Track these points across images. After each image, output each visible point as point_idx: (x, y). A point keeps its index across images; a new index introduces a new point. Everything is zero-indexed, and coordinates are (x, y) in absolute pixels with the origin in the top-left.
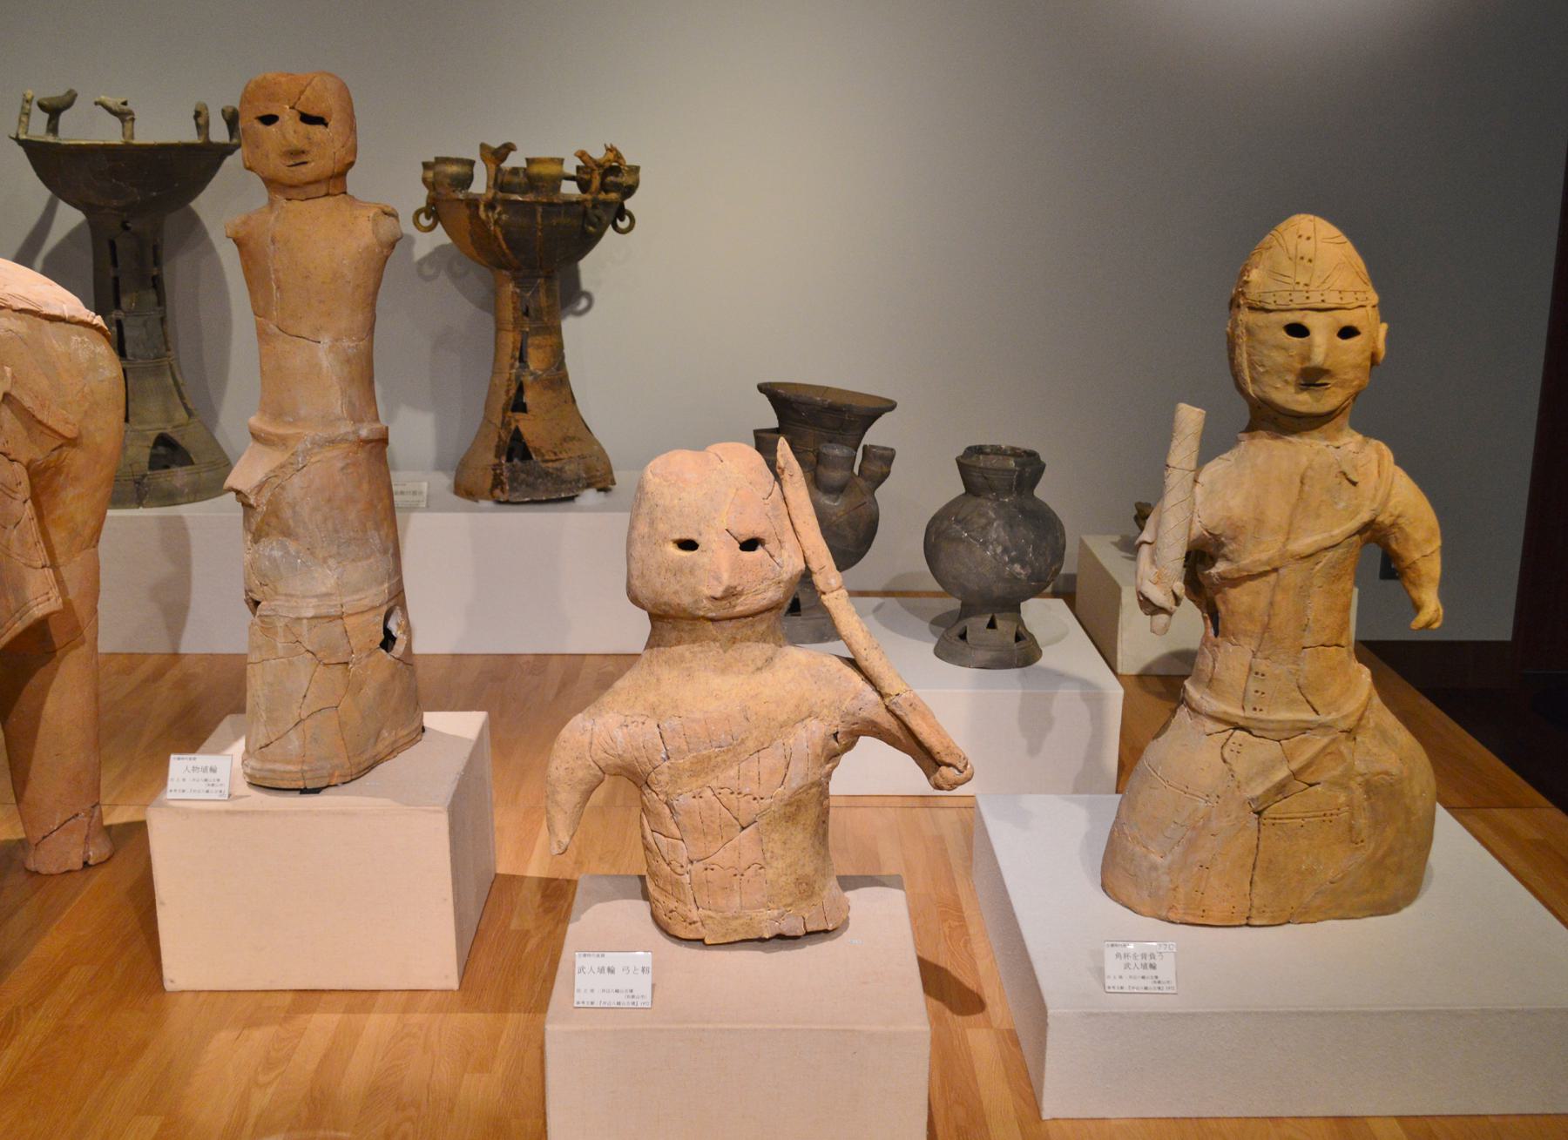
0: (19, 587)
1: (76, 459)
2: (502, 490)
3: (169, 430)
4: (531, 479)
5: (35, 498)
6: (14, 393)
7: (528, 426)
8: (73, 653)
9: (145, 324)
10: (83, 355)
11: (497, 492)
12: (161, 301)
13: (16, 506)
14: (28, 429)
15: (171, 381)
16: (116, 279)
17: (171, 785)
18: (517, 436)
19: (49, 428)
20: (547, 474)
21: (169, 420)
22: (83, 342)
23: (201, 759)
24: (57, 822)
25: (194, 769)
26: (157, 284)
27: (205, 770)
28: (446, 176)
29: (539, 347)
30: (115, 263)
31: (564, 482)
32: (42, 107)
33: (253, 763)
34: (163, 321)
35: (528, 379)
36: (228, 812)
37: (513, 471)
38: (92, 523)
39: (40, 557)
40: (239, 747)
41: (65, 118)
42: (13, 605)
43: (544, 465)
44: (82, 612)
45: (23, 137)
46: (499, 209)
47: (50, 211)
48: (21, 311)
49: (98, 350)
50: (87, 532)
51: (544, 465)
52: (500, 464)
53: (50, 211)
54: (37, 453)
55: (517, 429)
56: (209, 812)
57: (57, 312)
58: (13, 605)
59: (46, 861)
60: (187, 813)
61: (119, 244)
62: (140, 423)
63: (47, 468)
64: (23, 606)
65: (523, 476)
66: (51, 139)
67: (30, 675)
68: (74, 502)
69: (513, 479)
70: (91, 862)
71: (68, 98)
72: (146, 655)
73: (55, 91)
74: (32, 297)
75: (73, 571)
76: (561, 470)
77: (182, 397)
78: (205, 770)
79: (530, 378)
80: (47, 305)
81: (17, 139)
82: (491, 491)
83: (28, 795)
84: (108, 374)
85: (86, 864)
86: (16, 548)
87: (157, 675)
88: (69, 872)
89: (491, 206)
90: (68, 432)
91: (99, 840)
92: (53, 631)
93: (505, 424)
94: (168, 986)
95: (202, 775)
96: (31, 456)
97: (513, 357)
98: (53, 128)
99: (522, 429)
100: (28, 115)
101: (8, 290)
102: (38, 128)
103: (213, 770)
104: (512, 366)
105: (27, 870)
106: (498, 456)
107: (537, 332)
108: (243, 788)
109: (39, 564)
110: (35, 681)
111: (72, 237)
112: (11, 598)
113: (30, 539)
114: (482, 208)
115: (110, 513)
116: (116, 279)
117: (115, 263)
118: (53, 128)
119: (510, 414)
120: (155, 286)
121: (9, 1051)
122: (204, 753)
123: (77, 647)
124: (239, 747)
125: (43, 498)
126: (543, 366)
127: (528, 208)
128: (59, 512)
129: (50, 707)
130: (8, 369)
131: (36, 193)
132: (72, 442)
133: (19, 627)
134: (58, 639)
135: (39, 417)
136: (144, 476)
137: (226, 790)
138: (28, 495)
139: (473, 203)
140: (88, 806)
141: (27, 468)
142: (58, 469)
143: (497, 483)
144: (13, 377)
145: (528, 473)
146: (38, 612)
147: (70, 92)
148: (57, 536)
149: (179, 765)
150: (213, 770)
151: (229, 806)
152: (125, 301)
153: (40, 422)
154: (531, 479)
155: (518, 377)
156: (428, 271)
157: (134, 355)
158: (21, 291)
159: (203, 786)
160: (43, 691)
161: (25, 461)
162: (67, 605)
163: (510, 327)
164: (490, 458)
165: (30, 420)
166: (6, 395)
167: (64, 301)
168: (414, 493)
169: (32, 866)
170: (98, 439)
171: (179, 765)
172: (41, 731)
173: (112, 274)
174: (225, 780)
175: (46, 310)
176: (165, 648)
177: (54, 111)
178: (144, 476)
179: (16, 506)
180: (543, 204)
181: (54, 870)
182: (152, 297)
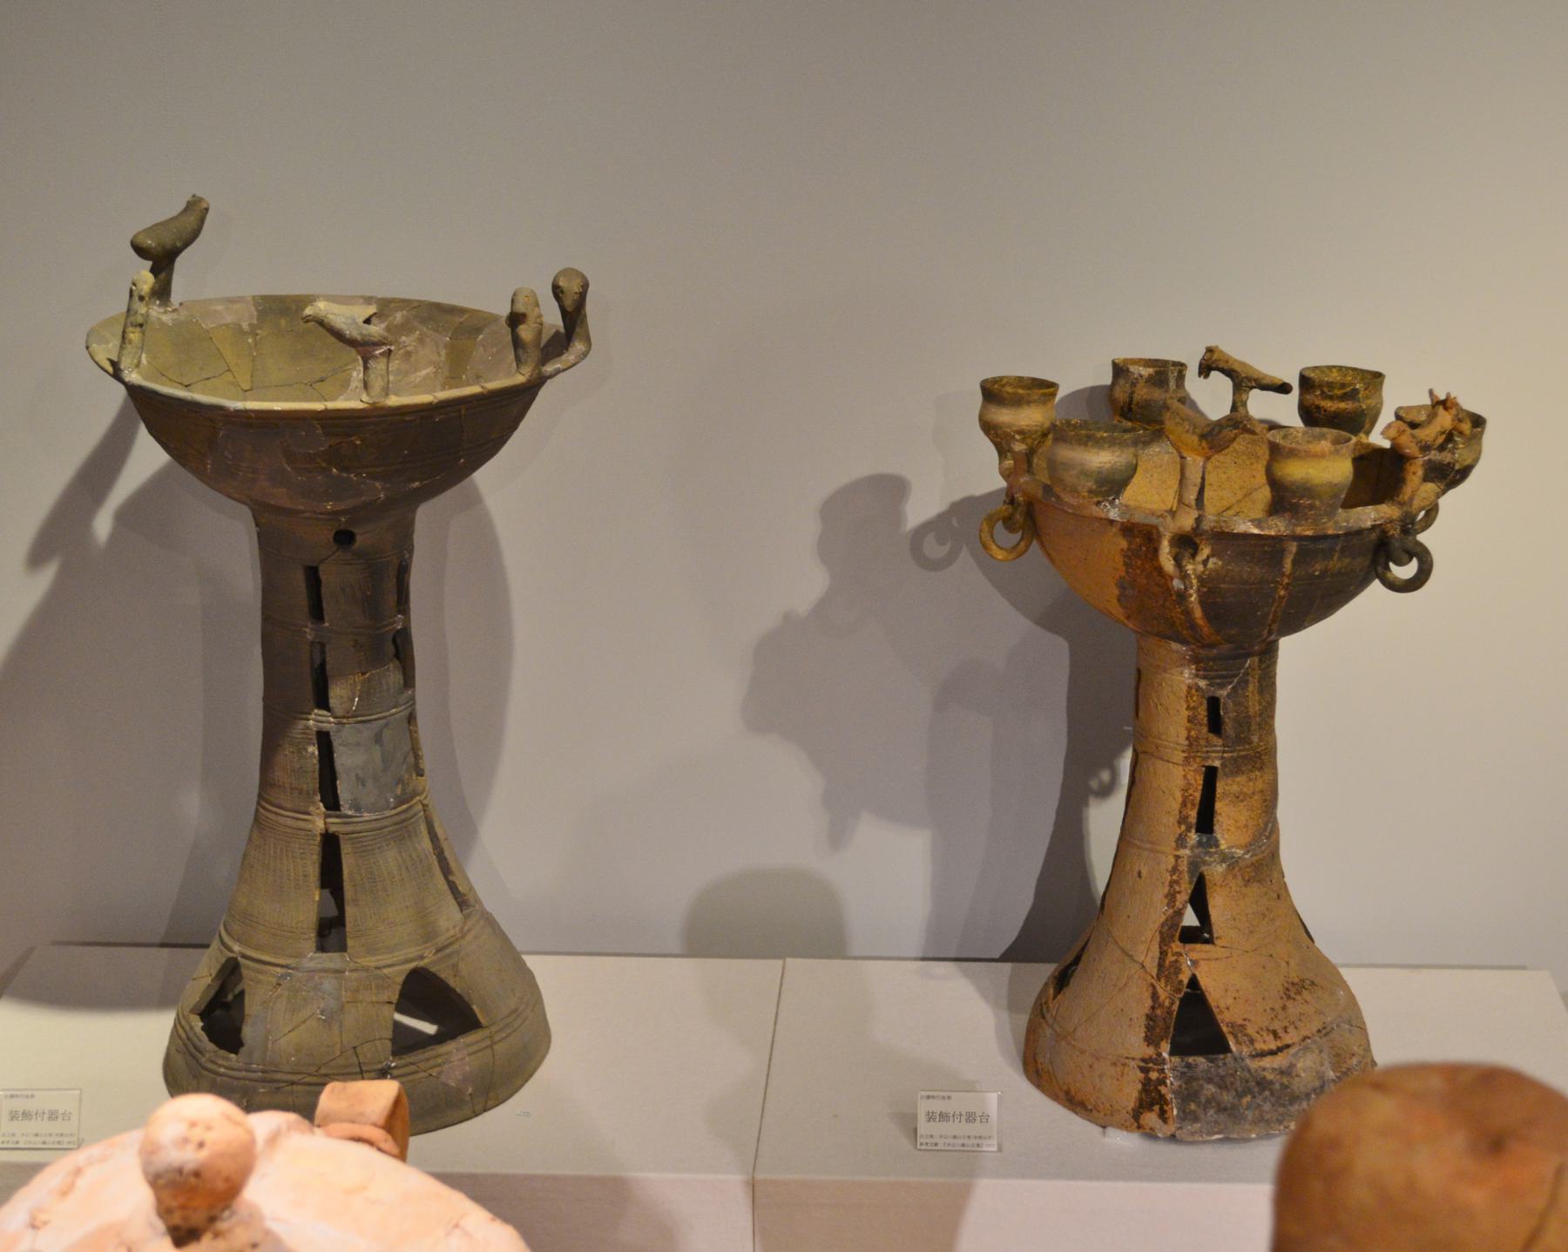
2: (1163, 1115)
3: (428, 960)
4: (1227, 1098)
7: (1222, 976)
9: (378, 739)
11: (1151, 1118)
12: (409, 681)
15: (426, 844)
18: (1194, 997)
20: (1263, 1084)
21: (429, 934)
26: (401, 650)
28: (1085, 473)
29: (1238, 798)
30: (317, 613)
31: (1294, 1099)
34: (411, 718)
35: (1215, 871)
37: (1188, 1076)
43: (1254, 1064)
46: (1205, 551)
51: (1254, 1064)
52: (1159, 1061)
55: (1194, 982)
61: (328, 576)
62: (372, 950)
65: (1210, 1089)
69: (1188, 1095)
71: (192, 219)
73: (159, 208)
76: (1286, 1072)
77: (446, 871)
79: (1221, 869)
82: (1137, 1114)
89: (1186, 543)
93: (1166, 969)
97: (1182, 820)
99: (1204, 982)
104: (1181, 841)
106: (1151, 1040)
107: (1236, 767)
114: (1165, 547)
119: (1177, 946)
120: (397, 656)
126: (1244, 838)
127: (1269, 549)
139: (1142, 536)
143: (1151, 1098)
145: (1223, 1086)
152: (338, 693)
154: (1227, 1098)
155: (1194, 865)
156: (933, 549)
157: (357, 808)
163: (1179, 756)
164: (1136, 1045)
168: (971, 1118)
180: (1300, 538)
182: (394, 677)
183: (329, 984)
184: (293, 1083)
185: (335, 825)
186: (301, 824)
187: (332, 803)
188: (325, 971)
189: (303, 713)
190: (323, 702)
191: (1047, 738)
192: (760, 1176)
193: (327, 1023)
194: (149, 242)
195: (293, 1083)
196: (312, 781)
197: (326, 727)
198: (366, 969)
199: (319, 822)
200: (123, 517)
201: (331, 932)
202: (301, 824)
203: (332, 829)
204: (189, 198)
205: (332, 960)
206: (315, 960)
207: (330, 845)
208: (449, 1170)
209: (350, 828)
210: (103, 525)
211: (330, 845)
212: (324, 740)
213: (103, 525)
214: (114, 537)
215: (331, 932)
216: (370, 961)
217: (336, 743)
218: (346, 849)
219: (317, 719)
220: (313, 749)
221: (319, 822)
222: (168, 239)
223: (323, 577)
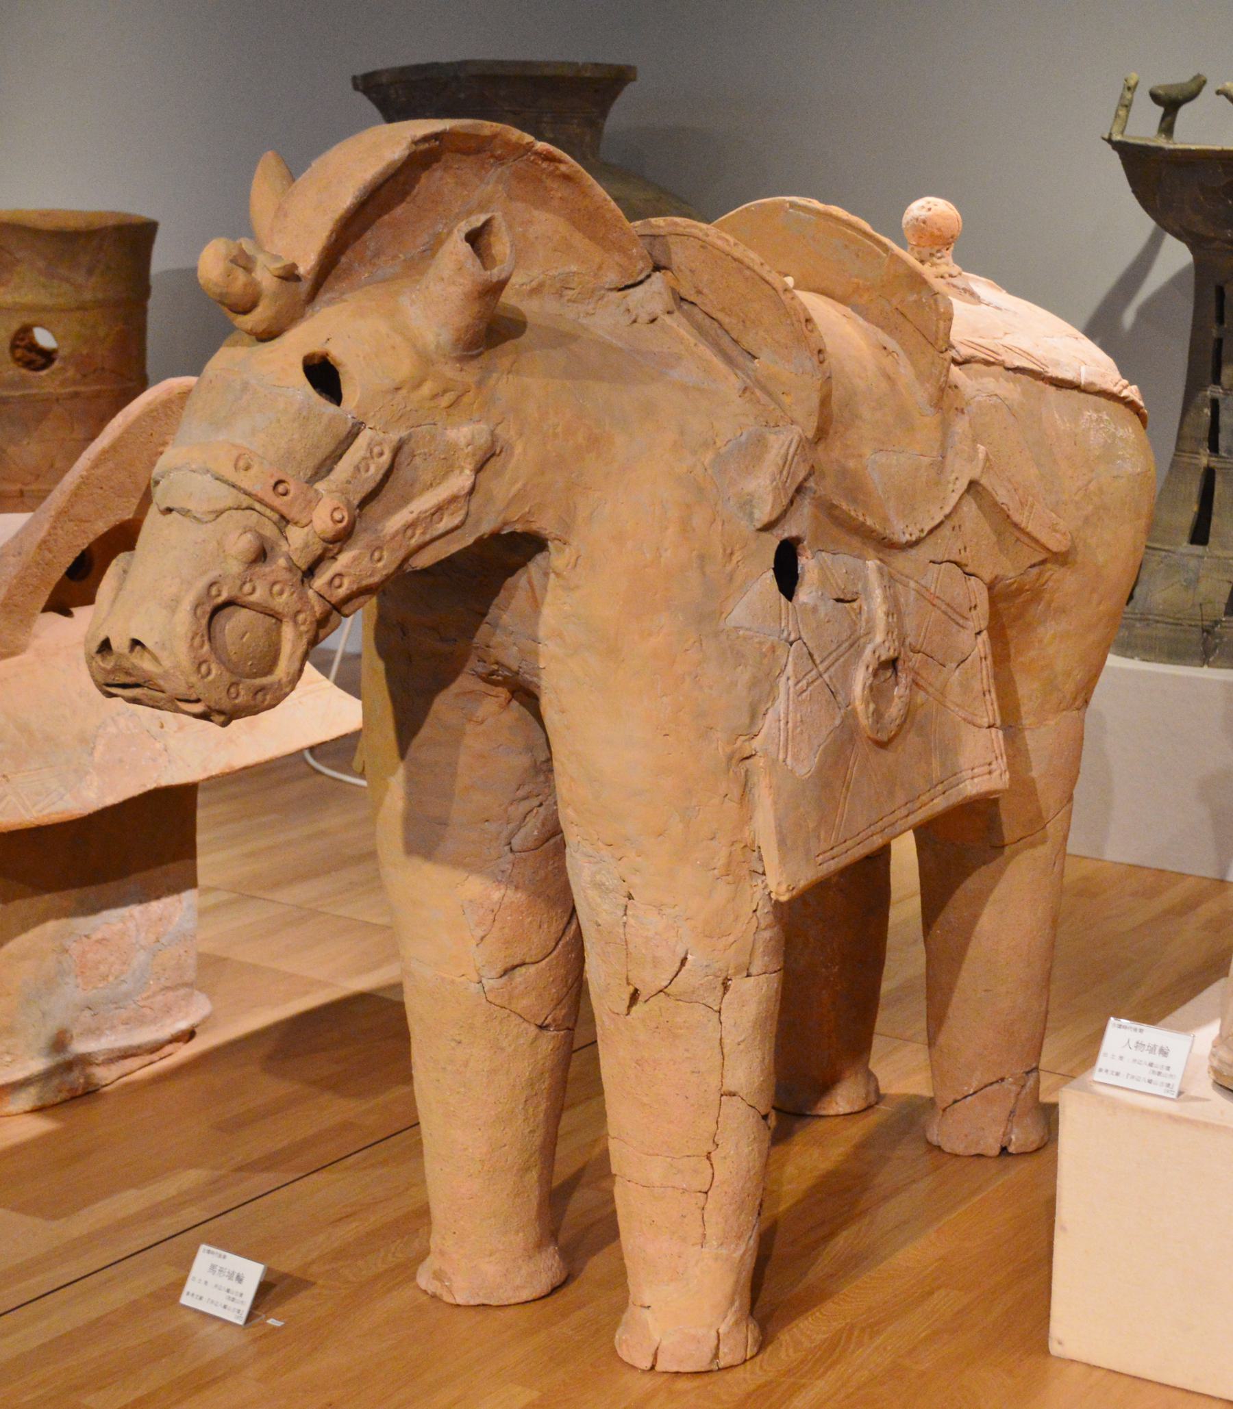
0: (949, 749)
1: (1064, 582)
5: (998, 631)
6: (984, 481)
8: (1028, 853)
10: (1096, 439)
13: (964, 639)
14: (999, 534)
16: (1219, 342)
17: (1102, 1062)
19: (1028, 535)
22: (1099, 420)
23: (1152, 1034)
24: (975, 1085)
25: (1139, 1045)
27: (1152, 1050)
30: (1220, 319)
32: (1155, 97)
33: (1223, 1053)
36: (1172, 1118)
38: (1079, 675)
39: (989, 711)
40: (1212, 1031)
41: (1184, 112)
42: (937, 773)
44: (1048, 798)
45: (1117, 137)
47: (1153, 246)
48: (1017, 370)
49: (1121, 432)
50: (1069, 687)
53: (1153, 246)
54: (1008, 569)
56: (1144, 1112)
57: (1068, 375)
58: (937, 773)
59: (951, 1133)
60: (1114, 1106)
62: (1225, 548)
63: (1020, 591)
64: (952, 776)
66: (1162, 142)
67: (966, 874)
68: (1052, 643)
70: (1012, 1149)
71: (1194, 87)
72: (1182, 876)
73: (1174, 76)
74: (1038, 353)
75: (1042, 739)
78: (1152, 1050)
80: (1057, 364)
81: (1109, 141)
83: (942, 1039)
84: (1128, 468)
85: (1004, 1150)
86: (954, 694)
87: (1188, 906)
88: (979, 1156)
90: (1055, 543)
91: (1028, 1121)
92: (1004, 817)
94: (1055, 1349)
95: (1146, 1056)
96: (999, 571)
98: (1167, 128)
100: (1128, 107)
101: (1008, 341)
102: (1144, 127)
103: (1164, 1052)
105: (928, 1143)
108: (1204, 1086)
109: (985, 722)
110: (971, 883)
111: (1176, 282)
112: (935, 763)
113: (977, 686)
115: (1113, 661)
116: (1219, 342)
117: (1220, 319)
118: (1167, 128)
121: (820, 1383)
122: (1166, 1027)
123: (1033, 845)
124: (1212, 1031)
125: (1011, 633)
128: (1033, 653)
129: (987, 922)
130: (981, 448)
131: (1139, 224)
132: (1062, 559)
133: (940, 804)
134: (1010, 830)
135: (1016, 518)
136: (1216, 623)
137: (1176, 1084)
138: (984, 624)
140: (1019, 1071)
141: (990, 587)
142: (1036, 594)
144: (987, 459)
146: (972, 787)
147: (1198, 77)
148: (1027, 689)
149: (1120, 1036)
150: (1164, 1052)
151: (1173, 1108)
153: (1016, 525)
157: (1229, 451)
158: (1024, 343)
159: (1145, 1072)
160: (981, 898)
161: (988, 577)
162: (1022, 784)
165: (1004, 523)
166: (973, 485)
167: (1089, 362)
169: (934, 1136)
170: (1101, 559)
171: (1120, 1036)
172: (971, 952)
173: (1215, 333)
174: (1178, 1071)
175: (1053, 372)
176: (1211, 873)
177: (1170, 104)
178: (1216, 623)
179: (964, 639)
181: (960, 1149)
183: (1193, 563)
184: (1158, 622)
185: (1214, 462)
186: (1194, 461)
187: (1214, 448)
188: (1192, 555)
189: (1203, 387)
190: (1216, 380)
191: (808, 1120)
192: (808, 484)
193: (1187, 588)
194: (1161, 92)
195: (1158, 622)
196: (1204, 432)
197: (1217, 395)
198: (1219, 558)
199: (1204, 459)
200: (1142, 313)
201: (1200, 534)
202: (1194, 461)
203: (1212, 465)
204: (1195, 74)
205: (1198, 549)
206: (1185, 547)
207: (1209, 476)
208: (531, 718)
209: (1223, 465)
210: (1129, 317)
211: (1209, 476)
212: (1215, 405)
213: (1129, 317)
214: (1136, 324)
215: (1200, 534)
216: (1219, 553)
217: (1222, 407)
218: (1218, 478)
219: (1212, 391)
220: (1207, 411)
221: (1204, 459)
222: (1174, 93)
223: (1227, 293)
